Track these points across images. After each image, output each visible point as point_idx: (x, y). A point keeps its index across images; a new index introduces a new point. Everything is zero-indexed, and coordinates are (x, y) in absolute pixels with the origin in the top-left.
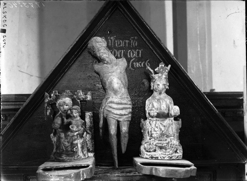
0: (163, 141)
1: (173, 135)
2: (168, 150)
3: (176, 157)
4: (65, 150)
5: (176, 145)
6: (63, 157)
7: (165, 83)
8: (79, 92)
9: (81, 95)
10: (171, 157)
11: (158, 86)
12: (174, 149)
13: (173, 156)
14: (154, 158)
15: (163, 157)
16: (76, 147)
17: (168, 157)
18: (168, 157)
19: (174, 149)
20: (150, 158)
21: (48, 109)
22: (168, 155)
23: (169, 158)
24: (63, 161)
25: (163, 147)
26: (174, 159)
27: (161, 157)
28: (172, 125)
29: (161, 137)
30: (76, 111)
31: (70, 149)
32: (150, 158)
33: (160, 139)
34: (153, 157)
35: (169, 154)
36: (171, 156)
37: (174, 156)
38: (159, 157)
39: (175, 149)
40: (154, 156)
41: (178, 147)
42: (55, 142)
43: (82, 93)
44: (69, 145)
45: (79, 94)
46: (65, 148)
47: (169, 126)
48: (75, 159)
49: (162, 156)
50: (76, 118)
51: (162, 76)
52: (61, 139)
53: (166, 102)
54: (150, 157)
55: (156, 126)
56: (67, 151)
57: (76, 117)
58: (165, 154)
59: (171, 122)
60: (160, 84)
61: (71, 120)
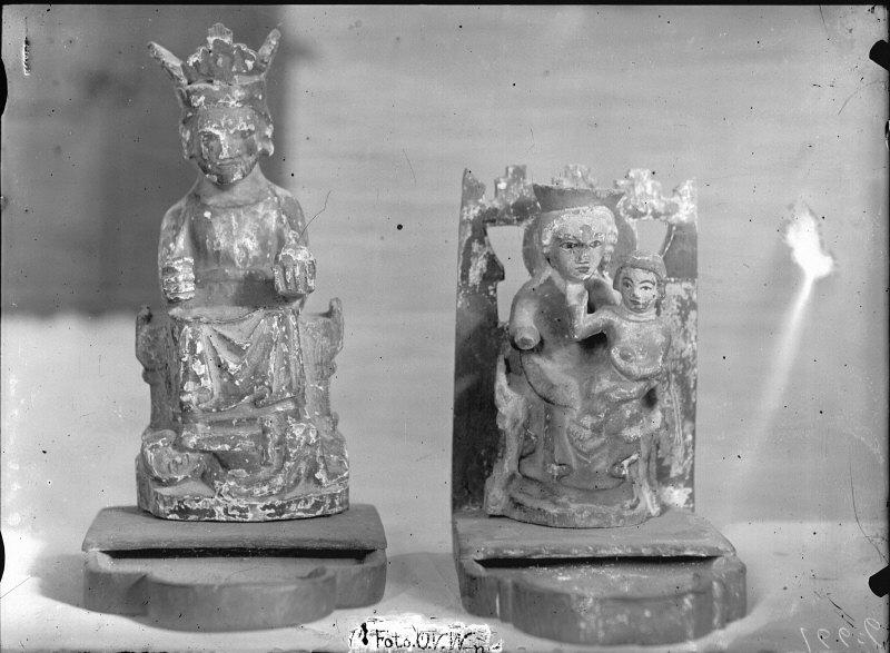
0: (238, 425)
1: (288, 395)
2: (263, 473)
3: (308, 506)
4: (574, 463)
5: (307, 444)
6: (564, 499)
7: (245, 128)
8: (639, 178)
9: (644, 194)
10: (282, 506)
11: (212, 143)
12: (297, 462)
13: (289, 504)
14: (192, 517)
15: (238, 508)
16: (634, 457)
17: (264, 509)
18: (264, 509)
19: (297, 462)
20: (176, 516)
21: (476, 255)
22: (262, 498)
23: (268, 511)
24: (565, 523)
25: (235, 455)
26: (299, 514)
27: (226, 511)
28: (285, 341)
29: (227, 403)
30: (651, 277)
31: (602, 465)
32: (170, 517)
33: (220, 417)
34: (187, 511)
35: (271, 494)
36: (278, 503)
37: (298, 502)
38: (219, 509)
39: (303, 467)
40: (196, 506)
41: (319, 452)
42: (515, 423)
43: (654, 186)
44: (597, 442)
45: (638, 190)
46: (578, 459)
47: (267, 351)
48: (622, 517)
49: (234, 502)
50: (639, 311)
51: (228, 91)
52: (557, 413)
53: (261, 222)
54: (172, 512)
55: (198, 351)
56: (587, 473)
57: (646, 305)
58: (250, 495)
59: (275, 325)
60: (217, 132)
61: (616, 320)
